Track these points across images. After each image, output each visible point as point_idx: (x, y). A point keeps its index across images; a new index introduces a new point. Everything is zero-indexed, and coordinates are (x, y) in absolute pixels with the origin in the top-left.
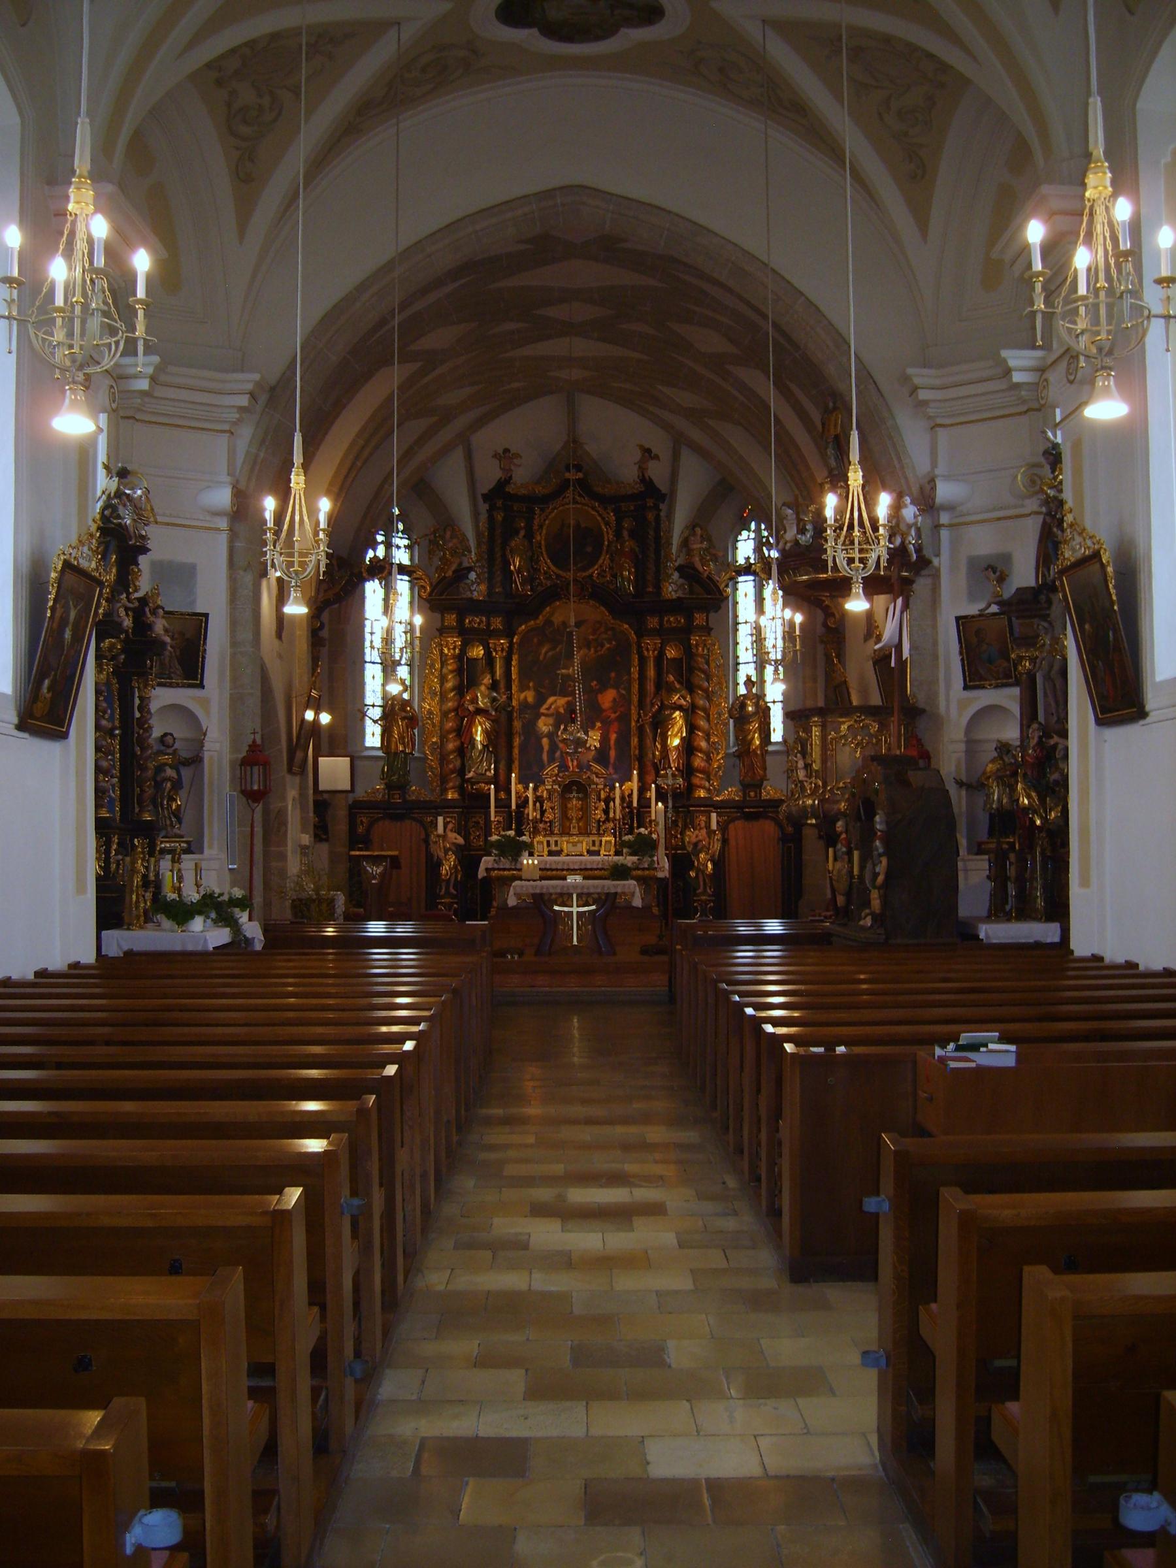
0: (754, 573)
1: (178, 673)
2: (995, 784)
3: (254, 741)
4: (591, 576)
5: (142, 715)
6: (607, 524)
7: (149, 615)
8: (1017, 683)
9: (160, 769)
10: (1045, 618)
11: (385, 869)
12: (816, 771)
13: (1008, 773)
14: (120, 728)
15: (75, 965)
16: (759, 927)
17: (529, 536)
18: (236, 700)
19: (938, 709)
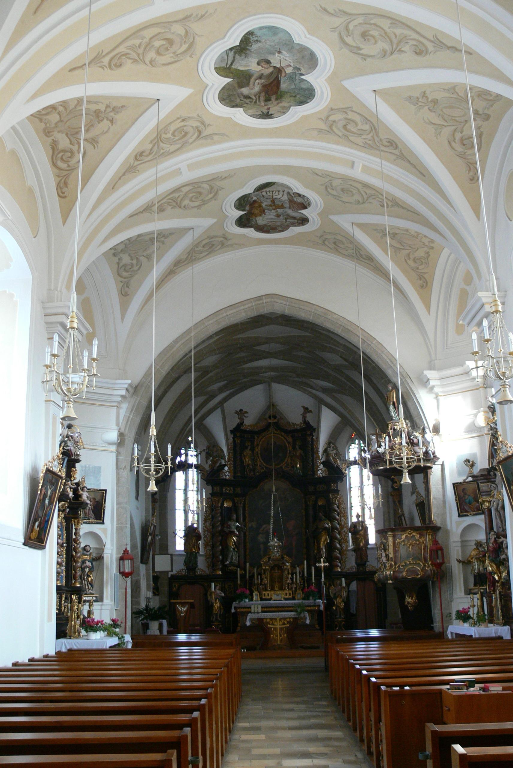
0: (358, 464)
1: (92, 517)
2: (476, 561)
3: (126, 549)
4: (282, 467)
5: (76, 537)
6: (289, 443)
7: (80, 490)
8: (483, 513)
9: (84, 562)
10: (494, 482)
11: (188, 609)
12: (391, 558)
13: (481, 556)
14: (66, 543)
15: (47, 656)
16: (367, 633)
17: (252, 450)
18: (120, 529)
19: (447, 526)
